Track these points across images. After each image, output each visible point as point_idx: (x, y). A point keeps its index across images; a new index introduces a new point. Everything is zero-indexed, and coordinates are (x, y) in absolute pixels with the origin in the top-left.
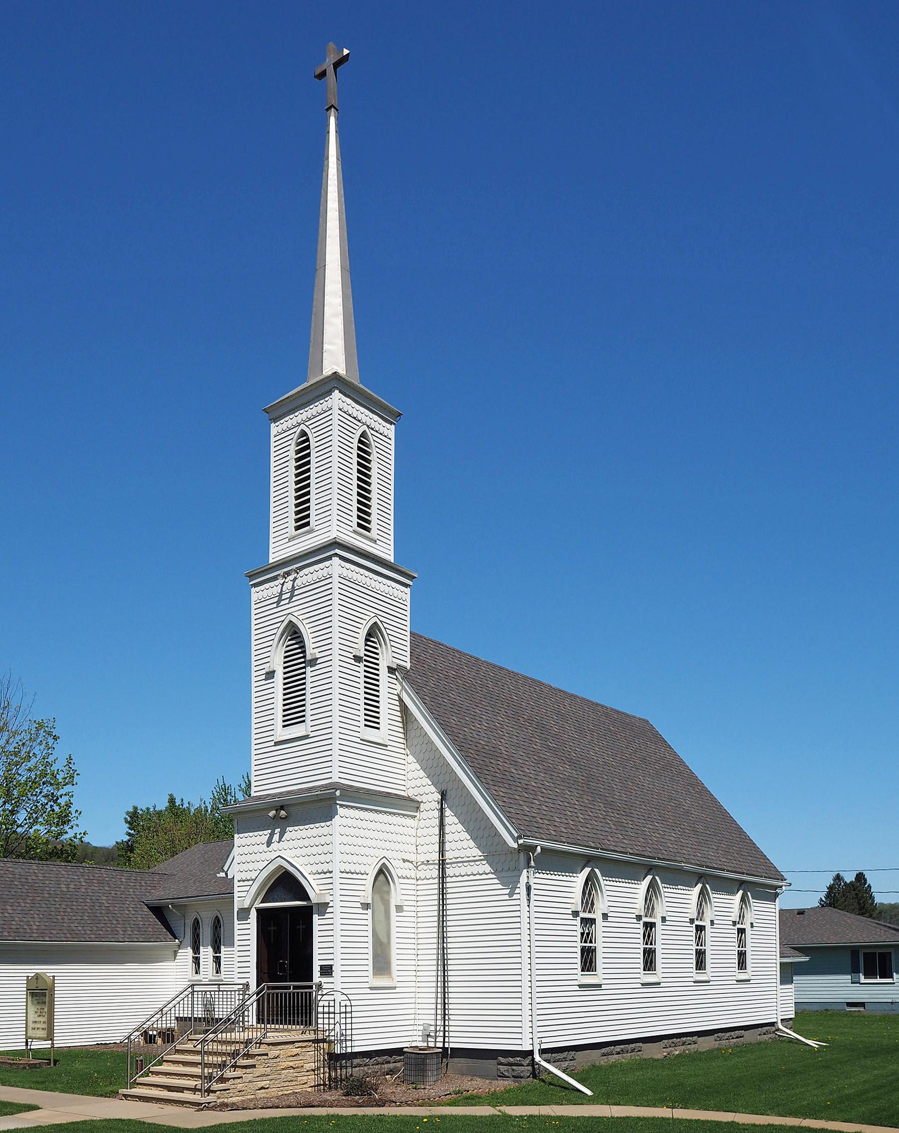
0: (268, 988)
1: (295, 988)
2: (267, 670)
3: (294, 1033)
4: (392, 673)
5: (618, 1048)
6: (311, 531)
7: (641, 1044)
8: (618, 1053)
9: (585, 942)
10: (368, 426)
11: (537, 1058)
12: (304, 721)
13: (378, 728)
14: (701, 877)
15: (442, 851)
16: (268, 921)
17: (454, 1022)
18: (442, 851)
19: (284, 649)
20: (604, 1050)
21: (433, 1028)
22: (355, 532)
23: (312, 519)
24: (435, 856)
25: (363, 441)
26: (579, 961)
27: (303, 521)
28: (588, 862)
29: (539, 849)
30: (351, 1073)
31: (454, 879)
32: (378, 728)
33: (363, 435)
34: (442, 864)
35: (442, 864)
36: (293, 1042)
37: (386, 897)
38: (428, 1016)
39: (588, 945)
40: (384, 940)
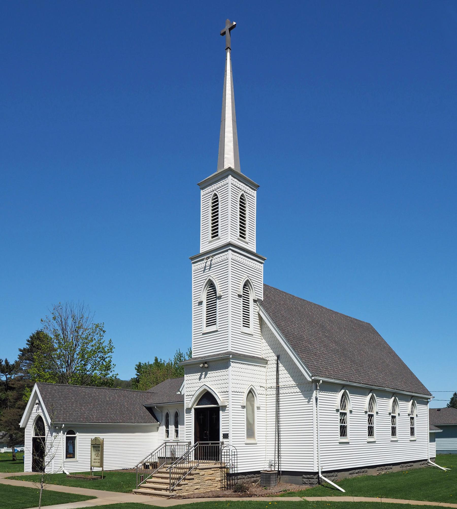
0: (200, 444)
1: (212, 444)
2: (199, 301)
7: (367, 469)
9: (342, 423)
12: (215, 324)
15: (278, 382)
18: (278, 382)
22: (238, 239)
24: (275, 385)
27: (215, 234)
29: (321, 381)
30: (237, 482)
33: (242, 195)
34: (278, 388)
35: (278, 388)
36: (211, 468)
38: (271, 456)
39: (343, 424)
40: (251, 422)
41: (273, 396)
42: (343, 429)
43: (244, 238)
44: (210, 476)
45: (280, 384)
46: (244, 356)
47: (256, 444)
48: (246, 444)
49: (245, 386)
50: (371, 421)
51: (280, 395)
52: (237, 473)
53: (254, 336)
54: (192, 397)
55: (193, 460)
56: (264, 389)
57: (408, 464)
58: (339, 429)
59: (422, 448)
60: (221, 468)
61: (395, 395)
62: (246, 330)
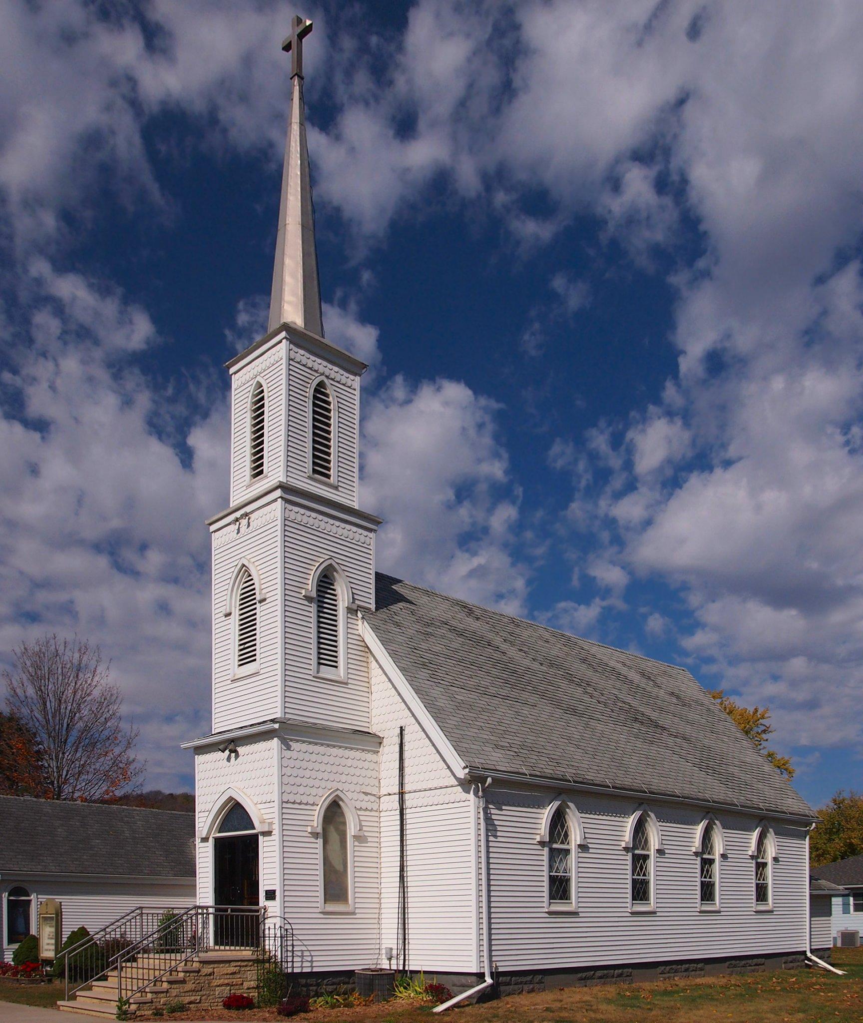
0: (232, 910)
1: (232, 910)
2: (224, 612)
3: (246, 953)
4: (352, 614)
5: (755, 961)
6: (266, 477)
7: (630, 970)
8: (791, 962)
9: (705, 877)
10: (327, 376)
11: (809, 954)
12: (255, 660)
13: (336, 667)
14: (761, 820)
15: (402, 784)
16: (223, 848)
17: (412, 946)
18: (402, 784)
19: (240, 592)
20: (579, 975)
21: (140, 966)
22: (310, 478)
23: (265, 467)
24: (396, 789)
25: (320, 389)
26: (754, 893)
27: (258, 471)
28: (560, 794)
29: (489, 780)
30: (294, 990)
31: (413, 810)
32: (336, 667)
33: (321, 384)
34: (402, 794)
35: (402, 794)
36: (230, 961)
37: (341, 827)
38: (390, 939)
39: (708, 880)
40: (339, 867)
41: (393, 813)
42: (561, 884)
43: (328, 476)
44: (228, 976)
45: (407, 788)
46: (325, 729)
47: (719, 912)
48: (700, 912)
49: (320, 792)
50: (761, 874)
51: (408, 811)
52: (301, 973)
53: (350, 686)
54: (206, 814)
55: (212, 943)
56: (373, 798)
57: (750, 961)
58: (754, 889)
59: (795, 927)
60: (257, 961)
61: (710, 815)
62: (326, 672)
